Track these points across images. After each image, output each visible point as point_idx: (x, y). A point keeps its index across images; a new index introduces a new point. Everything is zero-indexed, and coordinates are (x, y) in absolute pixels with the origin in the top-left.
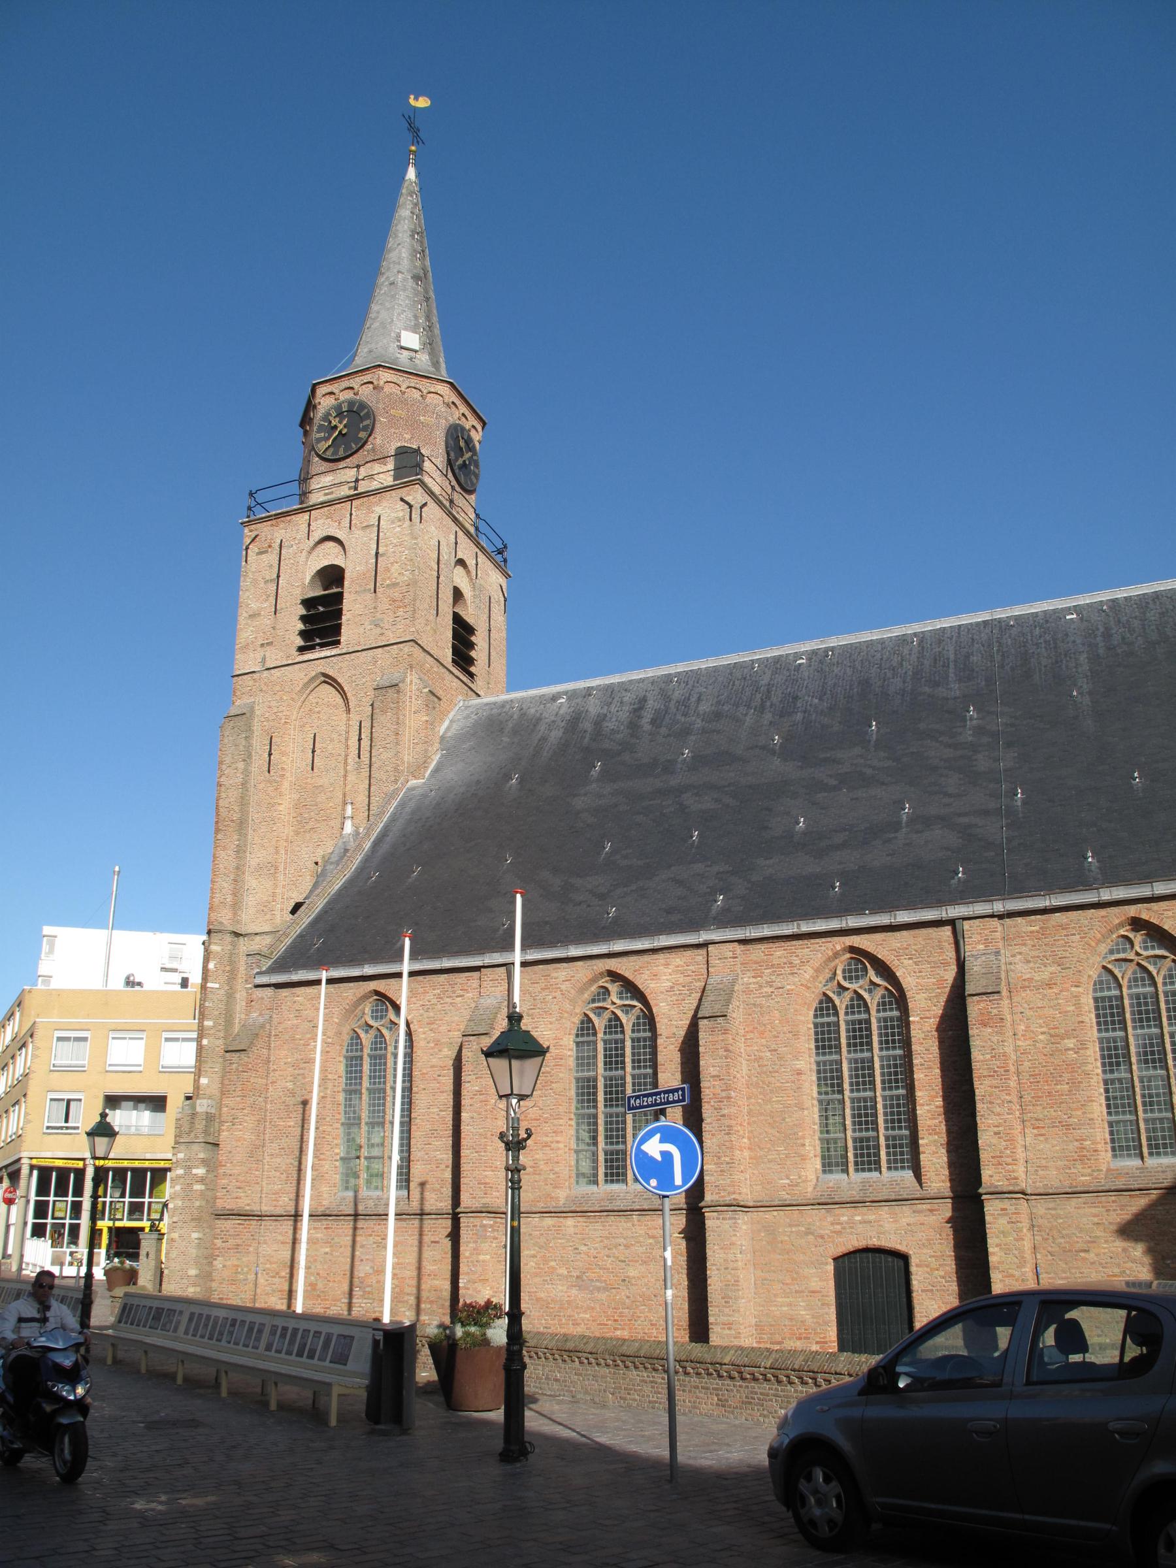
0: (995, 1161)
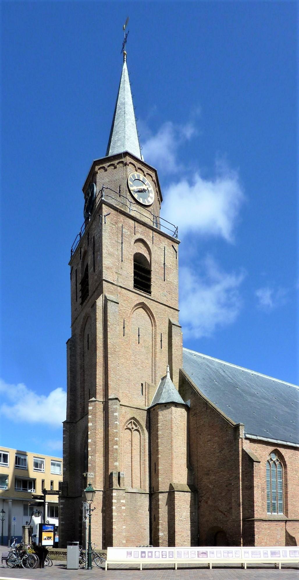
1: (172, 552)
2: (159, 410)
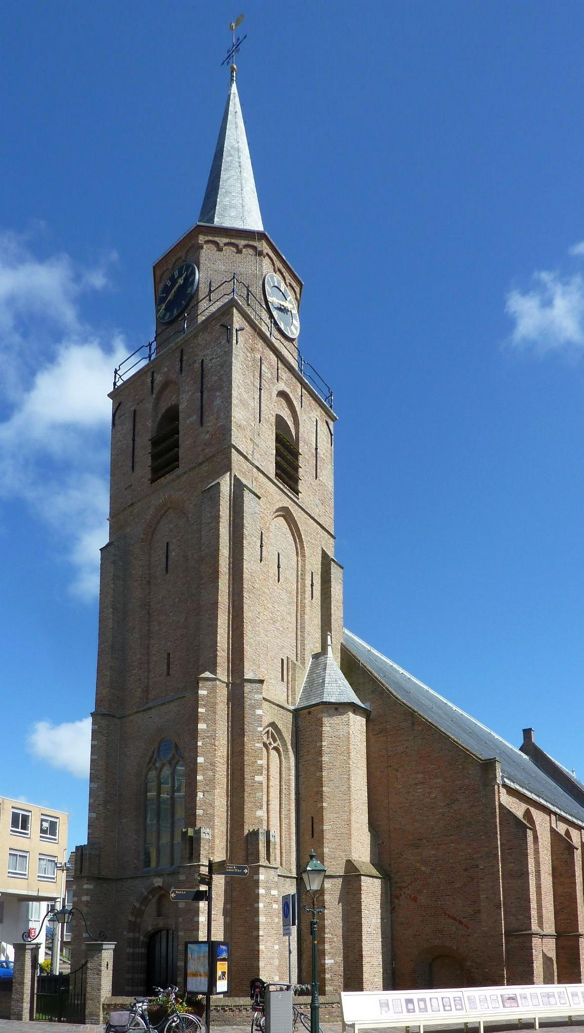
1: (459, 999)
2: (324, 715)
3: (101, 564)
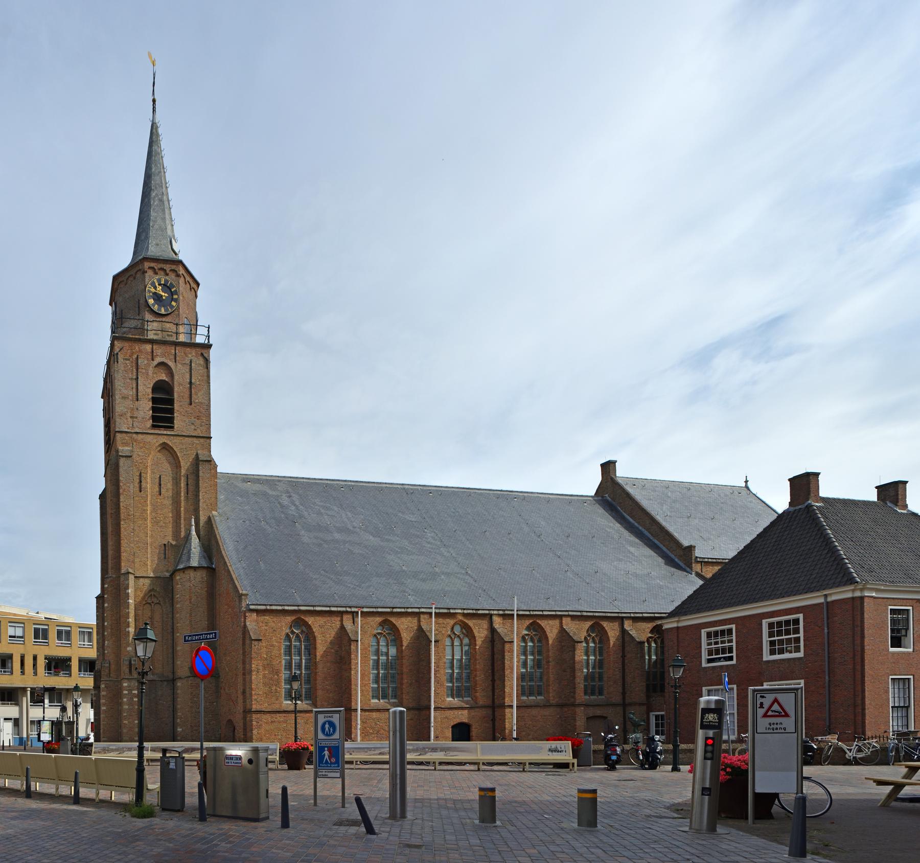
0: (509, 696)
3: (98, 598)
